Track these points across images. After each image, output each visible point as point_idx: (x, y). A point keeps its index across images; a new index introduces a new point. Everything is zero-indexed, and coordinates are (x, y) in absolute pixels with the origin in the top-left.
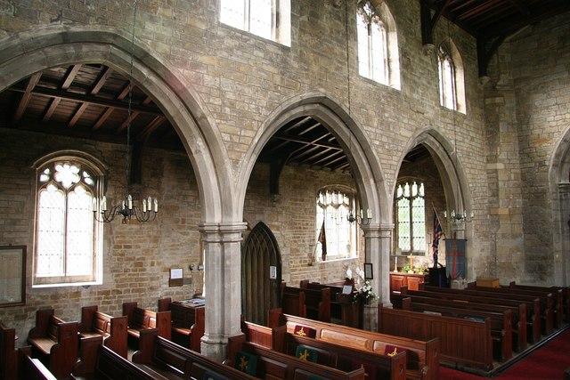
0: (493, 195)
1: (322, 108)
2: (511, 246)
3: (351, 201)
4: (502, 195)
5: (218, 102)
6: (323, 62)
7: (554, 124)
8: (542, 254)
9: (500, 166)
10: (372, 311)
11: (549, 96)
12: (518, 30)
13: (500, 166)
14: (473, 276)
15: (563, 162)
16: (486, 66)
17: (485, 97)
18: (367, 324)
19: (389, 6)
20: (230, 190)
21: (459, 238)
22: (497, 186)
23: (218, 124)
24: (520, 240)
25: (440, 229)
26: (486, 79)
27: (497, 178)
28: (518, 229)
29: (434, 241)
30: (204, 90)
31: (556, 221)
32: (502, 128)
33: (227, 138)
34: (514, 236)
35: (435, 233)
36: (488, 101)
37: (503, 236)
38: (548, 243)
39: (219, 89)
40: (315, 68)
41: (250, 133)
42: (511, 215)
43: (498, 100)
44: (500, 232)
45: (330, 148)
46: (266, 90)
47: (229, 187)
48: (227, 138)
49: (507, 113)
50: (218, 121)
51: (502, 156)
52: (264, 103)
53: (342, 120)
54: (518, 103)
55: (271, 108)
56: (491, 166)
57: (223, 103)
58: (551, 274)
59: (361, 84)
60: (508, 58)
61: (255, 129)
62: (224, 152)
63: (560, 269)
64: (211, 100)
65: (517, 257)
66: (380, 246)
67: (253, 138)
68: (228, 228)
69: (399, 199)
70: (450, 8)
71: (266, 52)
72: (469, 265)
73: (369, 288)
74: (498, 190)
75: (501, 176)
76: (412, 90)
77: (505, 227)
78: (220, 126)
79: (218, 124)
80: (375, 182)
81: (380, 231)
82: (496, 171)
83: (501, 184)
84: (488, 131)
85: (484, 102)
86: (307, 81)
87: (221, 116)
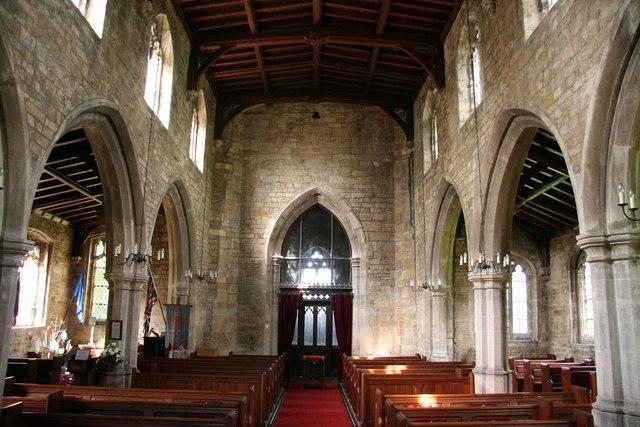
0: (213, 262)
1: (108, 124)
2: (225, 318)
3: (42, 253)
4: (221, 262)
5: (30, 71)
6: (122, 70)
7: (275, 200)
8: (254, 325)
9: (222, 233)
10: (118, 380)
11: (274, 174)
12: (254, 104)
13: (222, 233)
14: (194, 344)
15: (278, 236)
16: (222, 131)
17: (216, 161)
18: (561, 329)
19: (173, 38)
20: (23, 195)
21: (182, 303)
22: (218, 252)
23: (26, 100)
24: (234, 311)
25: (154, 294)
26: (220, 143)
27: (218, 244)
28: (233, 299)
29: (147, 308)
30: (18, 46)
31: (268, 292)
32: (229, 196)
33: (31, 121)
34: (229, 306)
35: (148, 299)
36: (218, 165)
37: (220, 305)
38: (260, 314)
39: (33, 53)
40: (115, 75)
41: (53, 126)
42: (228, 285)
43: (227, 166)
44: (216, 301)
45: (56, 177)
46: (74, 79)
47: (23, 190)
48: (31, 121)
49: (234, 181)
50: (26, 96)
51: (225, 223)
52: (70, 94)
53: (121, 144)
54: (245, 174)
55: (75, 102)
56: (213, 232)
57: (35, 74)
58: (261, 344)
59: (145, 110)
60: (241, 128)
61: (58, 122)
62: (27, 140)
63: (268, 340)
64: (24, 65)
65: (231, 327)
66: (132, 301)
67: (55, 134)
68: (16, 246)
69: (98, 258)
70: (213, 70)
71: (82, 34)
72: (190, 334)
73: (117, 350)
74: (218, 258)
75: (223, 244)
76: (175, 133)
77: (222, 296)
78: (29, 104)
79: (26, 100)
80: (135, 224)
81: (133, 282)
82: (218, 237)
83: (221, 251)
84: (214, 195)
85: (214, 166)
86: (108, 86)
87: (31, 90)
